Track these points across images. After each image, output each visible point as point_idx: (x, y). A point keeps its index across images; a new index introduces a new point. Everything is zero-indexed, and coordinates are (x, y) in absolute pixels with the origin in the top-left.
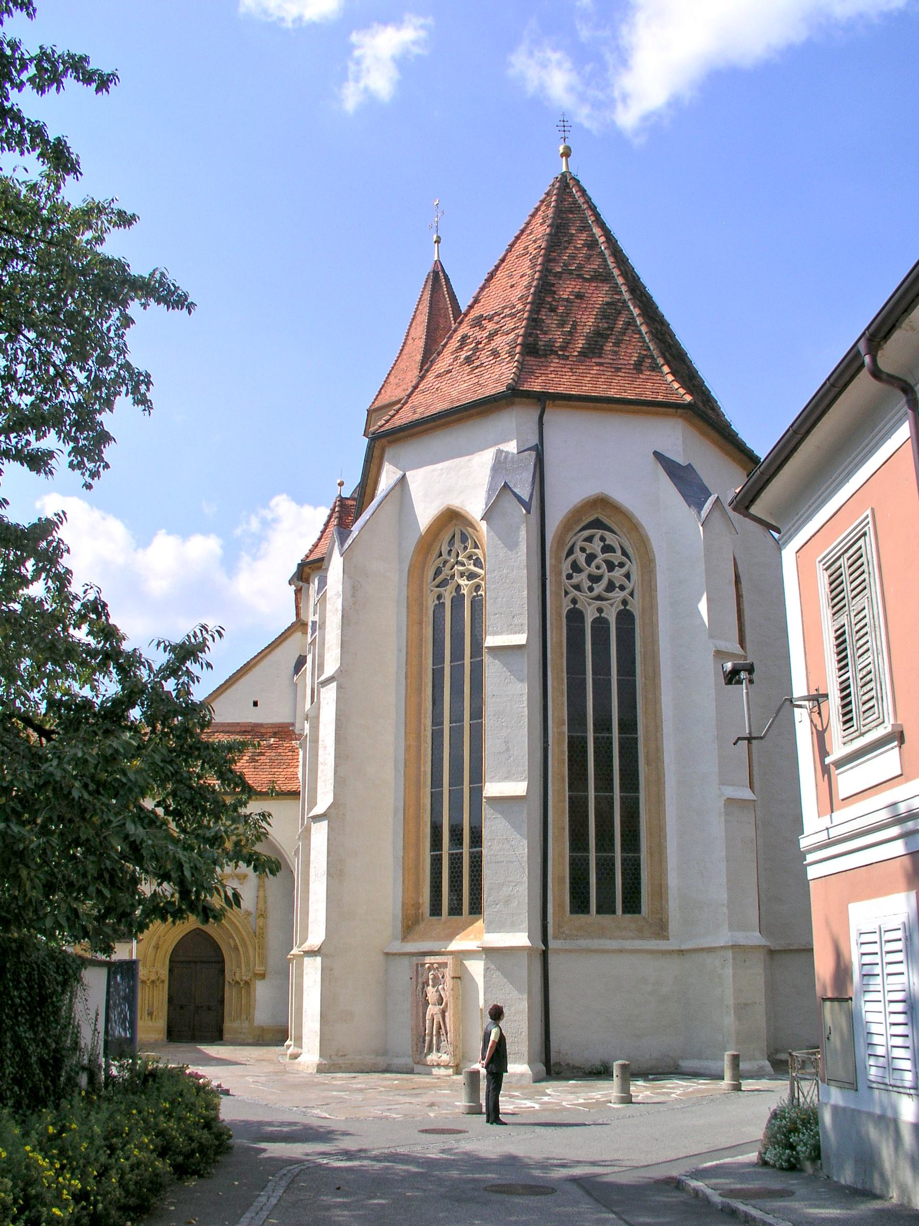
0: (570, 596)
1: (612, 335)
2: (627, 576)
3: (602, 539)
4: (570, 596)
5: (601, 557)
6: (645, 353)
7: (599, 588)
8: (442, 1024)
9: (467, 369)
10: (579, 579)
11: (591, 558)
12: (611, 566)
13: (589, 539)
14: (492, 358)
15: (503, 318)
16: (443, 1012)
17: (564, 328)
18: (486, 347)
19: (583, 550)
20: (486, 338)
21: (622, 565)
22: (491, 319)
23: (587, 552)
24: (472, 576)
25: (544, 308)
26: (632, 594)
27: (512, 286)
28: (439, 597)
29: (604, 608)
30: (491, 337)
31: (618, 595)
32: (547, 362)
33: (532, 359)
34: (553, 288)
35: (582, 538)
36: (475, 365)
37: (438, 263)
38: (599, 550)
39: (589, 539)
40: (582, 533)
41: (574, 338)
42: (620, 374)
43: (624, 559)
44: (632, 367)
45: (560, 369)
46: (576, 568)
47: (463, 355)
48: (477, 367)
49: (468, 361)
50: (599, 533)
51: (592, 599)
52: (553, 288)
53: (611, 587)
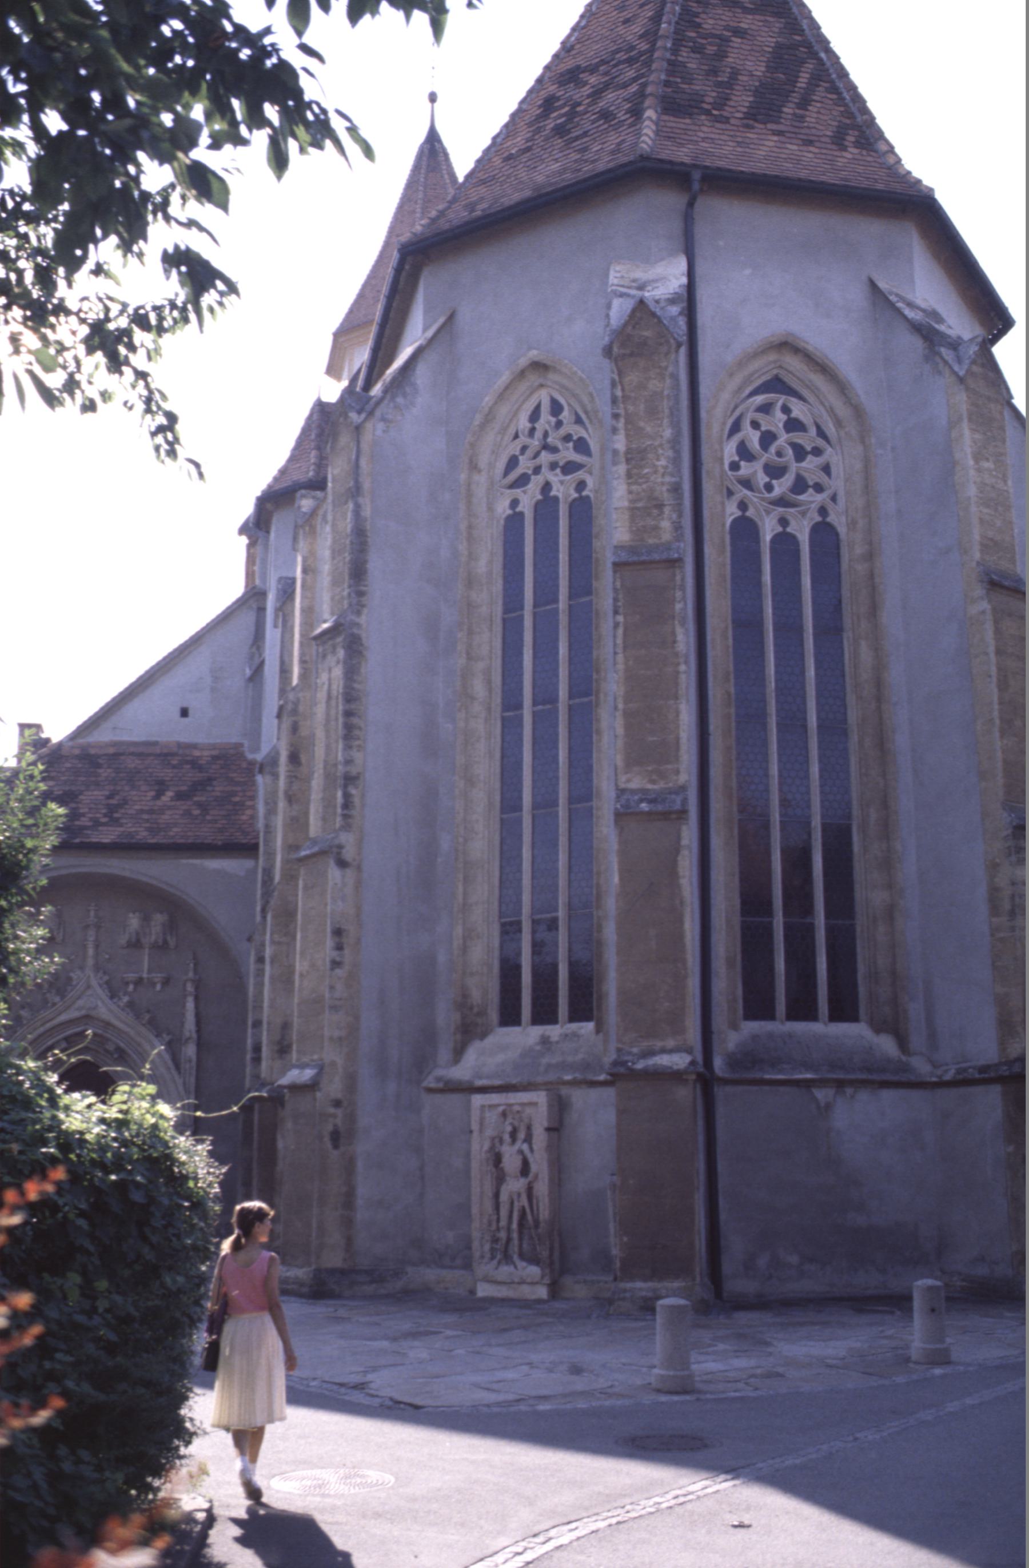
0: (737, 497)
1: (794, 92)
2: (826, 469)
3: (786, 410)
4: (737, 497)
5: (783, 438)
6: (848, 121)
7: (781, 486)
8: (528, 1210)
9: (559, 142)
10: (751, 471)
11: (768, 439)
12: (800, 453)
13: (766, 409)
14: (601, 122)
15: (615, 66)
16: (530, 1190)
17: (717, 76)
18: (590, 109)
19: (755, 425)
20: (588, 96)
21: (817, 452)
22: (593, 70)
23: (763, 428)
24: (569, 468)
25: (685, 46)
26: (834, 498)
27: (626, 21)
28: (515, 503)
29: (789, 518)
30: (597, 94)
31: (809, 497)
32: (695, 124)
33: (672, 119)
34: (697, 20)
35: (753, 408)
36: (573, 135)
37: (279, 177)
38: (781, 425)
39: (766, 409)
40: (751, 400)
41: (734, 92)
42: (812, 149)
43: (820, 442)
44: (828, 140)
45: (717, 136)
46: (744, 452)
47: (550, 124)
48: (577, 138)
49: (560, 131)
50: (781, 399)
51: (770, 503)
52: (697, 20)
53: (800, 485)
